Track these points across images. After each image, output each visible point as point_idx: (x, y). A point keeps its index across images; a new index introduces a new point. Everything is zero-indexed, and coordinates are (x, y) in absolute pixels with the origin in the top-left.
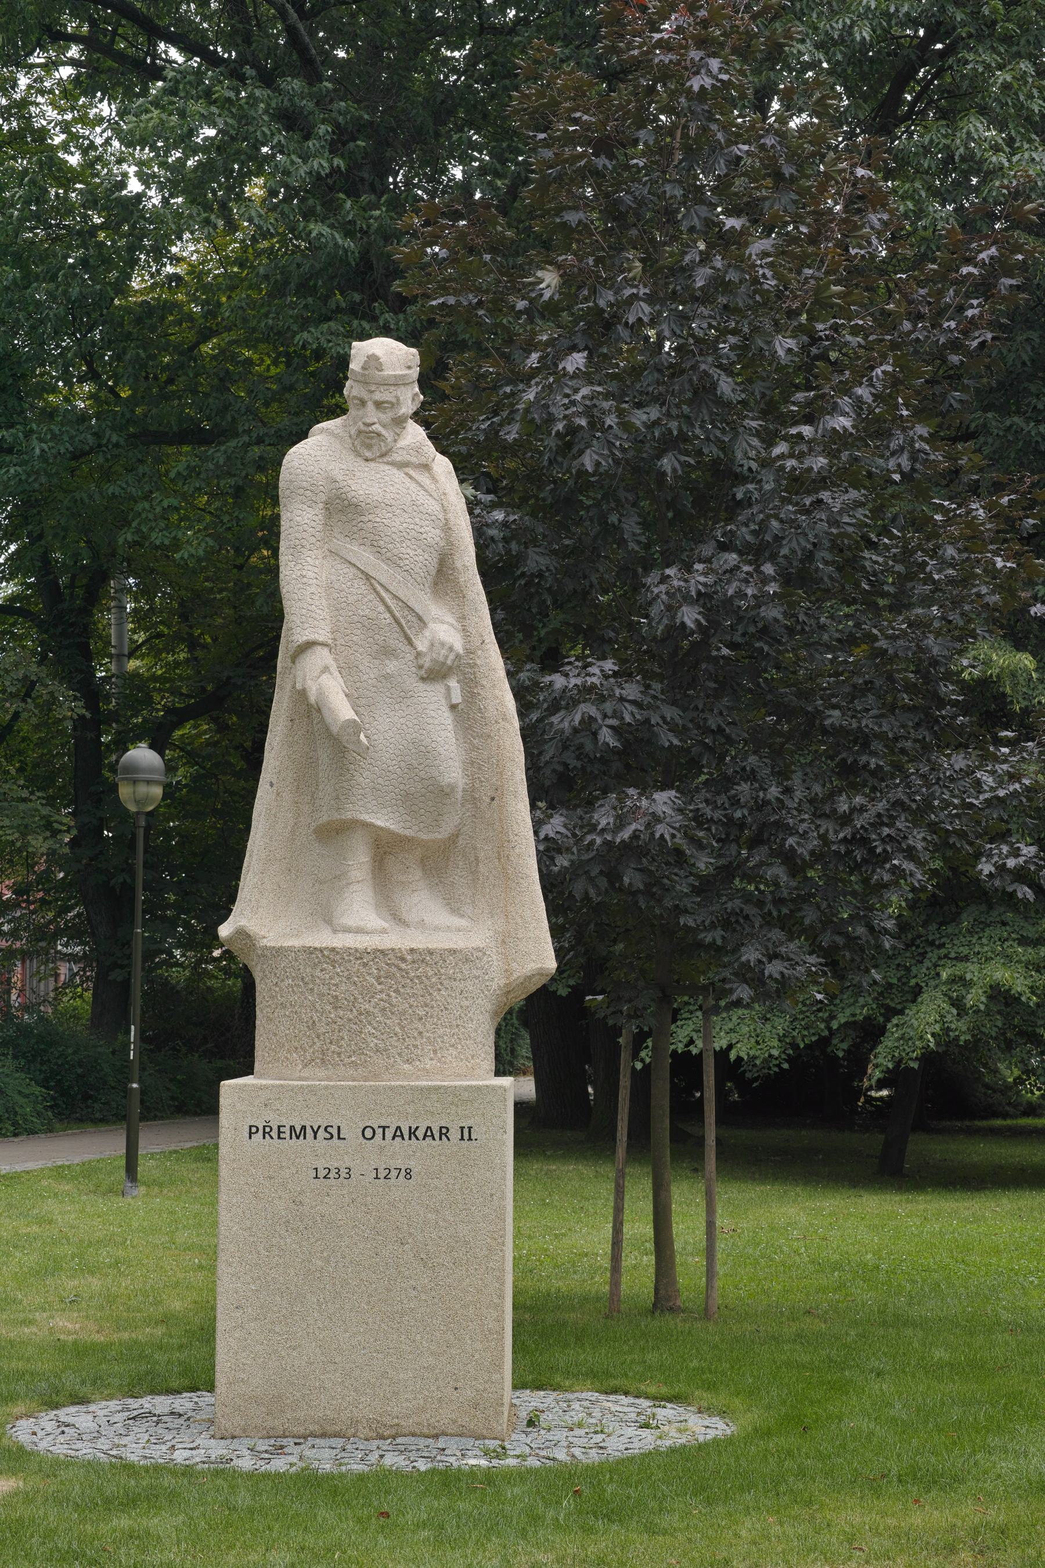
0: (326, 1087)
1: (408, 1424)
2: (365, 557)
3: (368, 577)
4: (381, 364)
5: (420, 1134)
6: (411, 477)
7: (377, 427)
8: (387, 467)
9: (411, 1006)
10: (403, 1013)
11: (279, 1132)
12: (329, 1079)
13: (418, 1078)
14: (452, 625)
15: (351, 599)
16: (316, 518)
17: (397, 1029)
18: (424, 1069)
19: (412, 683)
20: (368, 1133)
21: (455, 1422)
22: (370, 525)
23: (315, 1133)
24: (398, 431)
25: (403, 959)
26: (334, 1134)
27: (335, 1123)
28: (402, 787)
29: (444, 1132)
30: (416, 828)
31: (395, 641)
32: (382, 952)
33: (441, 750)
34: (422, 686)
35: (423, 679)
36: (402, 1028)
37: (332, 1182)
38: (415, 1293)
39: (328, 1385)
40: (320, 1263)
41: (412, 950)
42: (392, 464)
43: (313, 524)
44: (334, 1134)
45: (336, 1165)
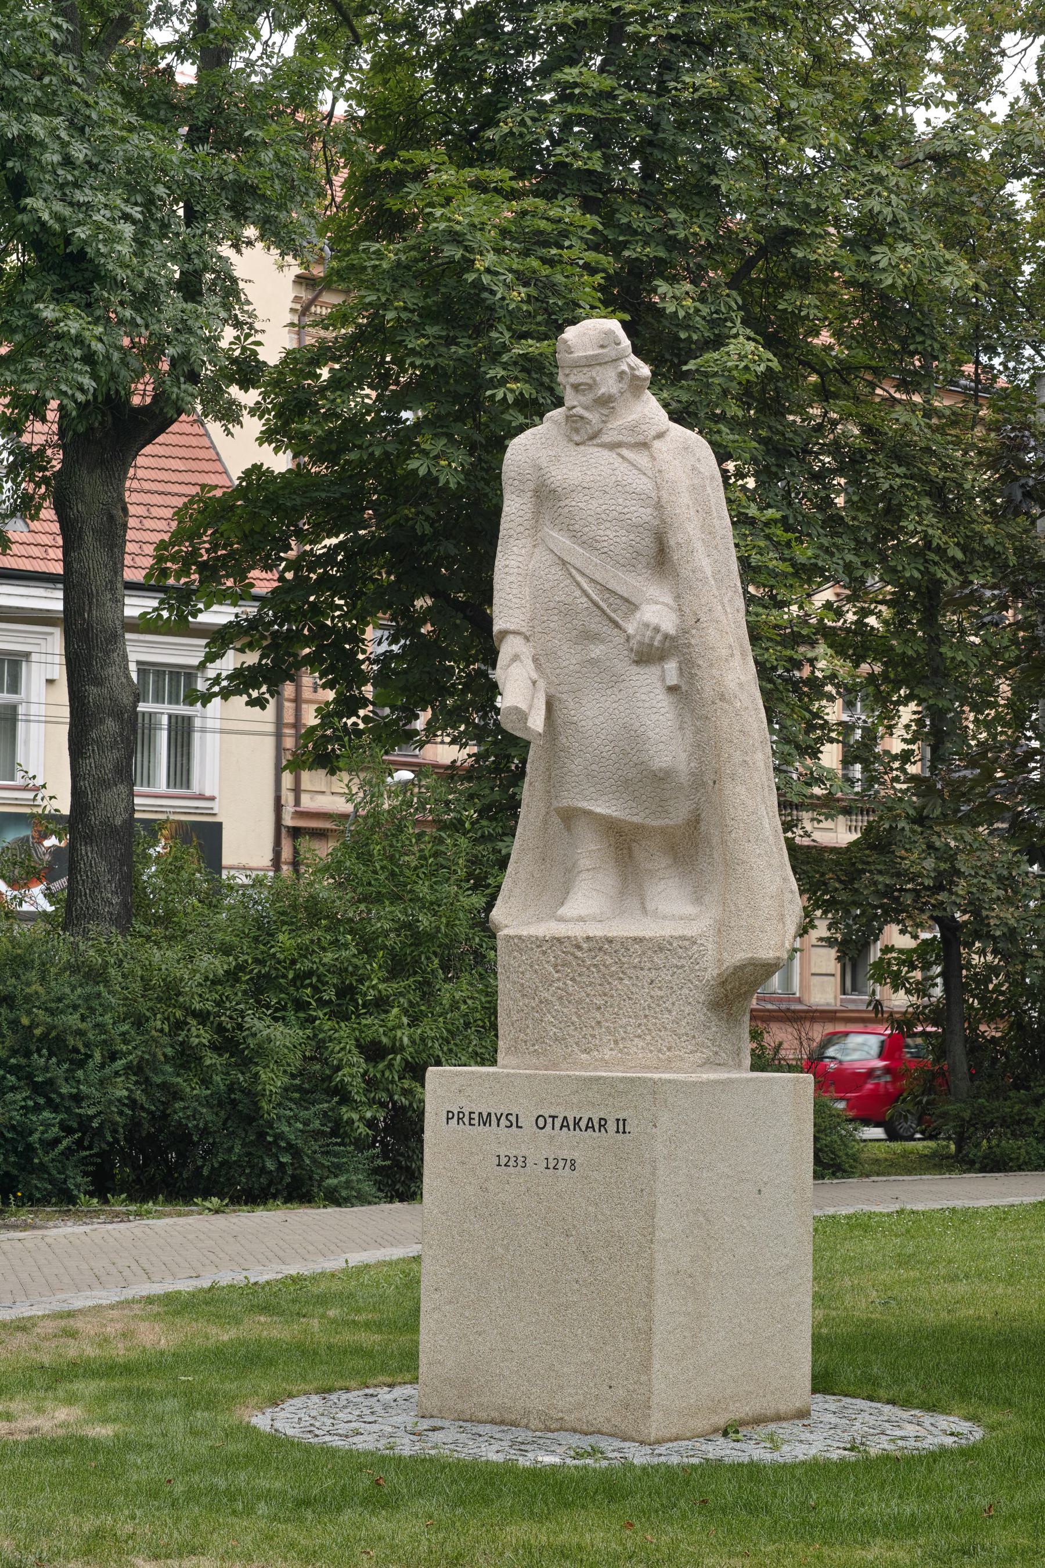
0: (508, 1075)
1: (570, 1419)
2: (560, 540)
3: (564, 563)
4: (569, 347)
5: (583, 1124)
6: (623, 457)
7: (579, 410)
8: (596, 449)
9: (588, 995)
10: (580, 1002)
11: (470, 1119)
12: (519, 1068)
13: (595, 1069)
14: (667, 605)
15: (547, 586)
16: (524, 507)
17: (574, 1018)
18: (602, 1059)
19: (623, 666)
20: (541, 1122)
21: (609, 1420)
22: (566, 510)
23: (499, 1120)
24: (605, 412)
25: (579, 947)
26: (513, 1122)
27: (515, 1111)
28: (620, 772)
29: (603, 1123)
30: (642, 814)
31: (596, 624)
32: (558, 940)
33: (651, 734)
34: (635, 669)
35: (637, 662)
36: (579, 1017)
37: (511, 1169)
38: (577, 1286)
39: (507, 1373)
40: (501, 1251)
41: (588, 938)
42: (603, 445)
43: (521, 513)
44: (513, 1122)
45: (515, 1153)
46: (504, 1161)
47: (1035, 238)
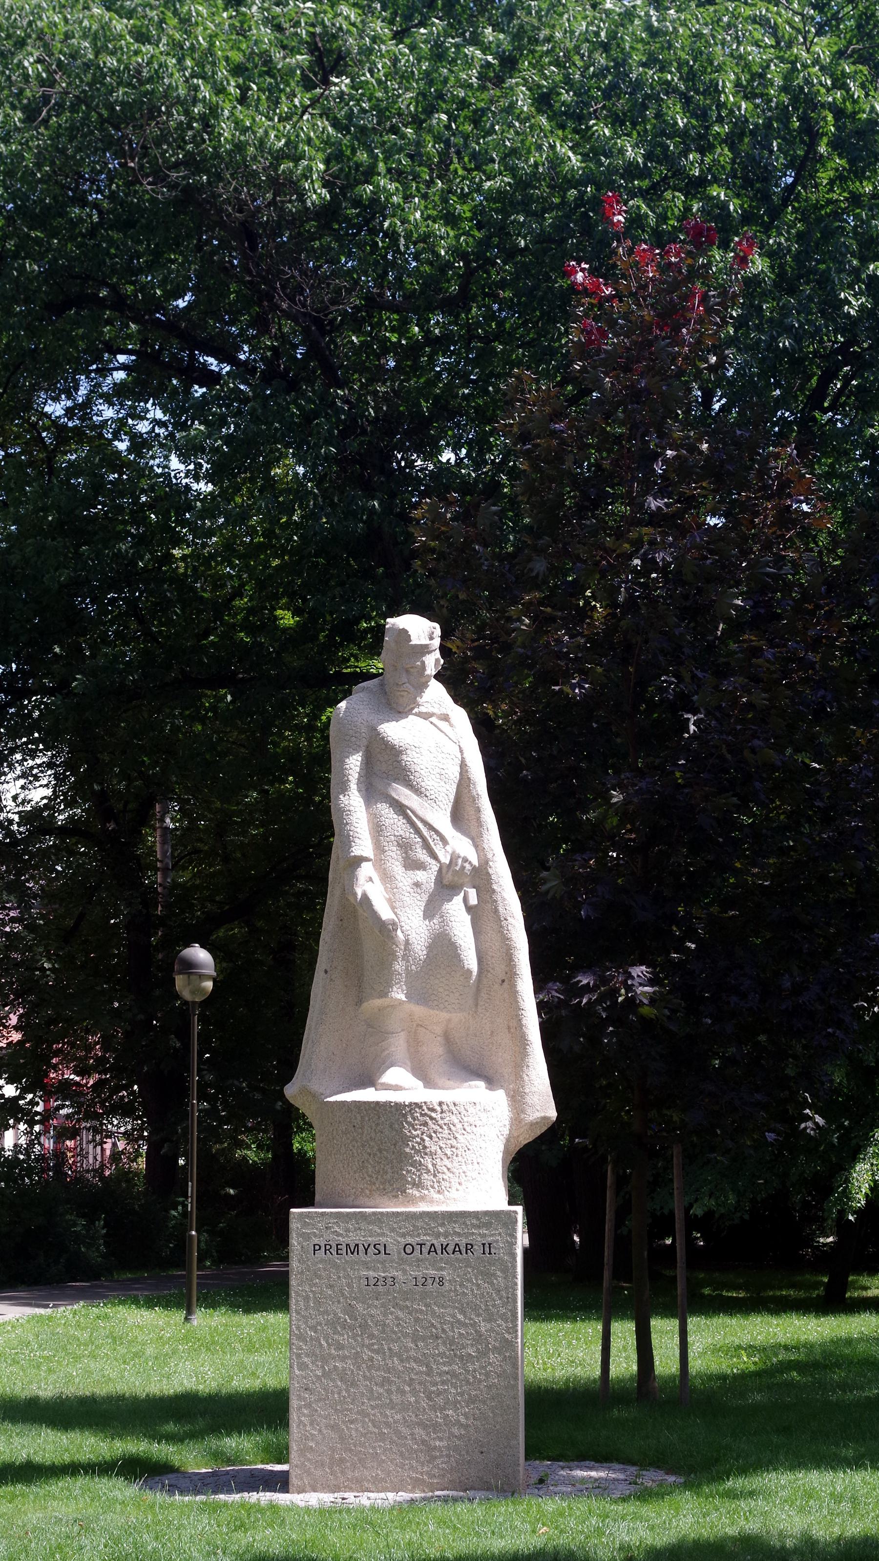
5: (450, 1249)
25: (433, 1110)
44: (381, 1250)
46: (372, 1282)
47: (864, 261)
